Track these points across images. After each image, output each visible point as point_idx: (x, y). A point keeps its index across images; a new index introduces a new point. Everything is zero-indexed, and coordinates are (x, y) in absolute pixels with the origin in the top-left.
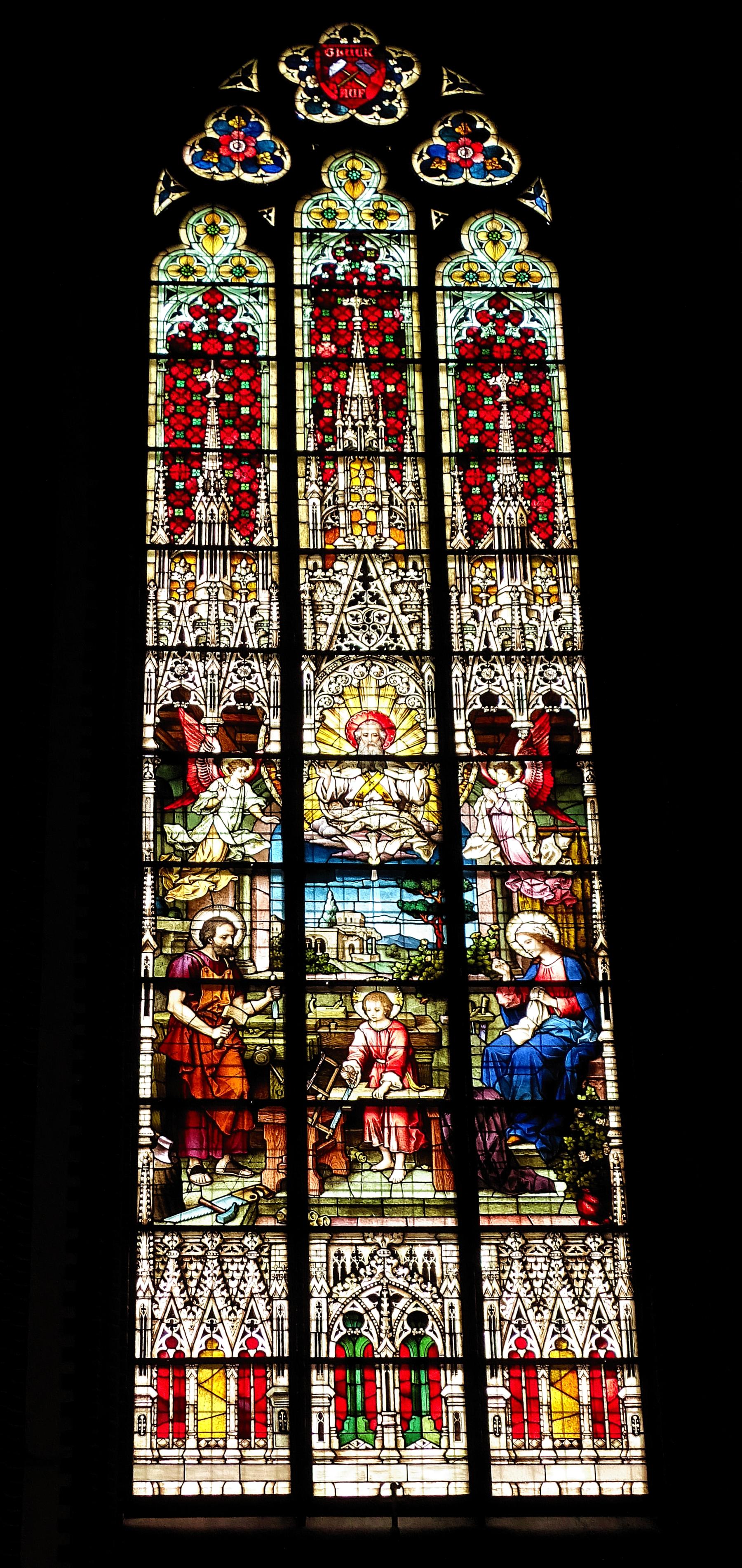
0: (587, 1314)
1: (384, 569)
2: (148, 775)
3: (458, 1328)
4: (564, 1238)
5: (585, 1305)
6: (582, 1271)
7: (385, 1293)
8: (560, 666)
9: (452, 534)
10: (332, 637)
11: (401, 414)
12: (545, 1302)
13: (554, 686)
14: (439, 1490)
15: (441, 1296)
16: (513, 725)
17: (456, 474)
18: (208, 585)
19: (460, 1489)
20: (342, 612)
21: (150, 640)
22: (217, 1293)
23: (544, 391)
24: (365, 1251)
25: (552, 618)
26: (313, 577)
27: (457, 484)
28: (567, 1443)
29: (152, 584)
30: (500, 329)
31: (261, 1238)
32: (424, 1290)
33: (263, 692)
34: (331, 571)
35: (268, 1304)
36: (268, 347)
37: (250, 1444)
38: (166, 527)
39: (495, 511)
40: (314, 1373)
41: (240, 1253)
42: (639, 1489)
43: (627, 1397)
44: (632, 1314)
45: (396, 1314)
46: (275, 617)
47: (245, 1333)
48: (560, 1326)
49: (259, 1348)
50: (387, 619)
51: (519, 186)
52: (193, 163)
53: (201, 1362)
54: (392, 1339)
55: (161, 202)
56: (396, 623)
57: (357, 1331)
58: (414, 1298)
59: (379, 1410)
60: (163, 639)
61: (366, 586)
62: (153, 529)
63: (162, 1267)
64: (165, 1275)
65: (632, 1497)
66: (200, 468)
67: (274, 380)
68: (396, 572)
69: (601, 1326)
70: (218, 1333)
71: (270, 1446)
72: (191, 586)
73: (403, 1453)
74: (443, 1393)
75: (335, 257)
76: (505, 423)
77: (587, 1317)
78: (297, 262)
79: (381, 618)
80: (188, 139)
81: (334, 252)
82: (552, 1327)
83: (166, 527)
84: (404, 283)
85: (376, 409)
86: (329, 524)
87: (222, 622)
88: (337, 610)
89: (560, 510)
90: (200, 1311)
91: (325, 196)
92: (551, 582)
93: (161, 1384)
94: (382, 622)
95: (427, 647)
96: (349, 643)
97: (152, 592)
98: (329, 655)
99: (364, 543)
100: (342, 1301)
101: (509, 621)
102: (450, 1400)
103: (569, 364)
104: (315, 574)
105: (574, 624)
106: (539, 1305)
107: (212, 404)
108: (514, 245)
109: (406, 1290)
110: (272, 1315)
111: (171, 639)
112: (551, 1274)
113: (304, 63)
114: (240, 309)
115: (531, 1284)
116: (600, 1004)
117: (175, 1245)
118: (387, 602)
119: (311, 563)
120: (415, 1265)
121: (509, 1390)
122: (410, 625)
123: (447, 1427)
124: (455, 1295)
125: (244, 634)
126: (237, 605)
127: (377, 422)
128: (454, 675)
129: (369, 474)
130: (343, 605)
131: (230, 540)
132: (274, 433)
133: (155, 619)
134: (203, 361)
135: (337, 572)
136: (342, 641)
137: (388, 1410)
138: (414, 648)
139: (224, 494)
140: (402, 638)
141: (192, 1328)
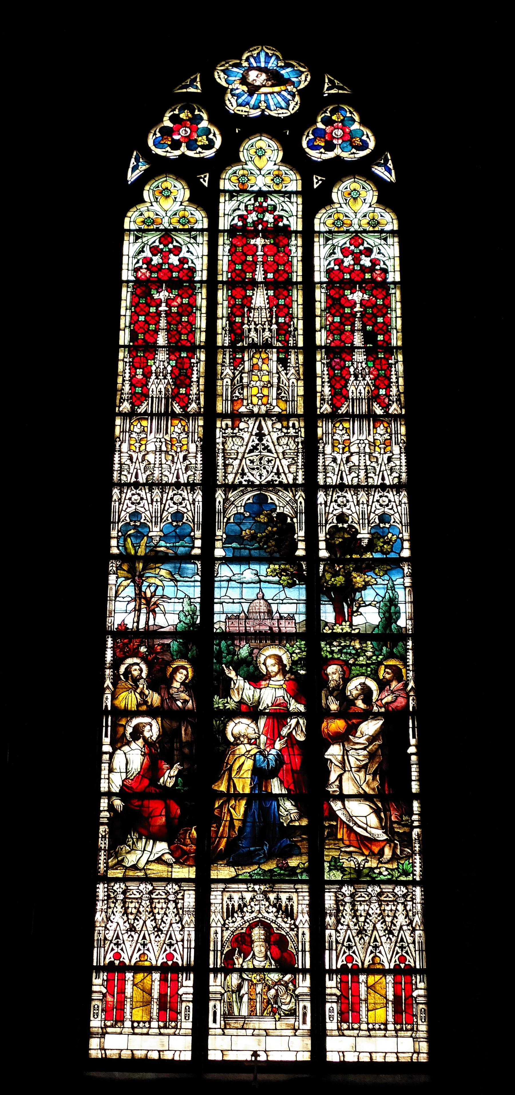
0: (394, 939)
1: (273, 428)
5: (162, 931)
8: (185, 494)
9: (121, 402)
10: (236, 474)
12: (366, 932)
14: (290, 1057)
15: (297, 927)
16: (359, 536)
23: (191, 303)
26: (225, 433)
30: (357, 260)
32: (286, 923)
33: (397, 515)
34: (237, 429)
37: (177, 1025)
39: (351, 388)
42: (423, 1058)
44: (423, 939)
46: (404, 464)
47: (165, 950)
50: (273, 462)
55: (133, 172)
56: (279, 465)
61: (260, 440)
62: (321, 404)
63: (112, 905)
64: (344, 914)
65: (419, 1063)
66: (351, 360)
67: (204, 296)
68: (280, 430)
69: (170, 945)
70: (148, 950)
71: (179, 1027)
75: (246, 210)
79: (269, 461)
80: (151, 128)
81: (246, 207)
82: (139, 945)
84: (293, 228)
85: (271, 316)
86: (236, 396)
87: (368, 467)
88: (240, 457)
90: (137, 935)
91: (241, 167)
93: (109, 983)
94: (270, 464)
96: (247, 479)
97: (321, 447)
100: (232, 929)
101: (357, 464)
102: (184, 996)
104: (227, 431)
105: (401, 466)
108: (369, 200)
114: (375, 249)
115: (357, 919)
117: (121, 890)
118: (274, 451)
119: (224, 423)
120: (280, 905)
121: (340, 991)
122: (289, 467)
124: (192, 925)
127: (271, 326)
130: (244, 453)
133: (324, 465)
135: (241, 430)
136: (242, 478)
138: (291, 482)
140: (283, 475)
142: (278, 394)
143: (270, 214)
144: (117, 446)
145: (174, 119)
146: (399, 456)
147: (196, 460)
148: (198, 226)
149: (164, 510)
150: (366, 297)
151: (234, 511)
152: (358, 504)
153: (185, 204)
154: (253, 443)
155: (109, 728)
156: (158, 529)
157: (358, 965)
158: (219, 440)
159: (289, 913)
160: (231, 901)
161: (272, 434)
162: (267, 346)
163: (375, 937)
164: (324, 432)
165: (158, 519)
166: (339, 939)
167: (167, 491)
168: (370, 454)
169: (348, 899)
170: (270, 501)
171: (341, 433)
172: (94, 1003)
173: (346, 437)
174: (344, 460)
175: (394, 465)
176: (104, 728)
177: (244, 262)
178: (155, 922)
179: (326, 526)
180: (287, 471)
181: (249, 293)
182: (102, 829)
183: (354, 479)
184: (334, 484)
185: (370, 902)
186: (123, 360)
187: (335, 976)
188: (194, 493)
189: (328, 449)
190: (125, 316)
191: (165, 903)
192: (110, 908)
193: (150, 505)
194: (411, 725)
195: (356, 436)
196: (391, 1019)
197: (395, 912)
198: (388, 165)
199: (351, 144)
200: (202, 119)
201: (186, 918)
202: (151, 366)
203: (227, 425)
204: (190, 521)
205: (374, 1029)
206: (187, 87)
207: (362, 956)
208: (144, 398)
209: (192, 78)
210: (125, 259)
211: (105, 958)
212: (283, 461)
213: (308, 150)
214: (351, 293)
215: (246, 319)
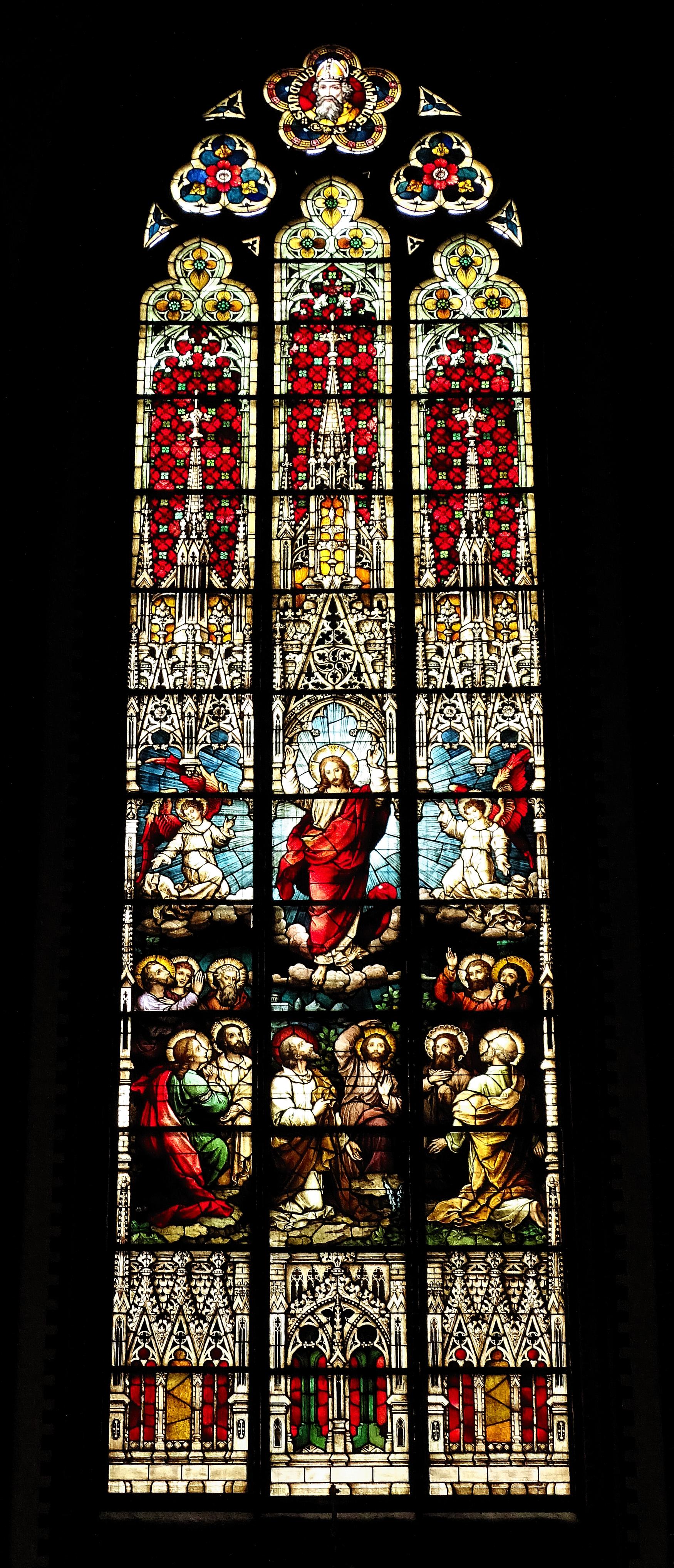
0: (522, 1327)
6: (518, 1288)
11: (511, 448)
12: (484, 1317)
18: (472, 625)
19: (401, 1489)
21: (132, 683)
27: (427, 523)
28: (499, 1447)
29: (420, 626)
32: (374, 1306)
35: (230, 1318)
36: (249, 385)
38: (433, 570)
45: (347, 1327)
47: (527, 1345)
48: (180, 1337)
49: (467, 1359)
52: (398, 193)
57: (312, 1345)
58: (364, 1313)
59: (331, 1417)
61: (333, 626)
63: (136, 1284)
64: (140, 1292)
68: (361, 611)
69: (533, 1339)
72: (170, 629)
73: (294, 1457)
74: (389, 1402)
76: (472, 458)
78: (277, 297)
79: (346, 656)
82: (489, 1339)
83: (150, 570)
84: (380, 317)
87: (199, 664)
89: (522, 544)
90: (170, 1324)
91: (303, 224)
92: (512, 617)
98: (299, 694)
101: (471, 657)
102: (395, 1408)
104: (286, 613)
107: (472, 443)
109: (357, 1306)
110: (234, 1329)
115: (157, 1299)
116: (543, 1033)
117: (220, 1263)
118: (352, 642)
120: (366, 1283)
121: (129, 1397)
122: (373, 663)
124: (402, 1310)
126: (213, 647)
128: (418, 712)
131: (494, 581)
132: (253, 472)
133: (138, 661)
134: (459, 399)
136: (309, 680)
138: (377, 686)
141: (163, 1339)
142: (358, 560)
143: (346, 296)
144: (134, 635)
145: (425, 156)
147: (244, 657)
148: (513, 313)
149: (142, 729)
150: (482, 417)
154: (323, 631)
155: (129, 1036)
156: (193, 755)
159: (379, 1294)
160: (297, 1277)
162: (342, 490)
163: (496, 1323)
164: (425, 613)
167: (493, 701)
168: (489, 643)
171: (505, 613)
173: (454, 618)
174: (510, 651)
175: (523, 658)
177: (309, 367)
178: (195, 1307)
179: (137, 748)
180: (370, 670)
183: (236, 681)
184: (207, 687)
186: (140, 512)
187: (283, 1381)
188: (242, 703)
190: (418, 446)
192: (133, 1287)
193: (529, 720)
194: (545, 1030)
195: (183, 618)
196: (517, 1437)
197: (524, 1290)
198: (513, 220)
200: (244, 157)
202: (460, 519)
203: (286, 604)
204: (178, 744)
205: (174, 1449)
206: (224, 109)
209: (231, 97)
210: (412, 363)
213: (397, 199)
214: (187, 412)
215: (312, 450)
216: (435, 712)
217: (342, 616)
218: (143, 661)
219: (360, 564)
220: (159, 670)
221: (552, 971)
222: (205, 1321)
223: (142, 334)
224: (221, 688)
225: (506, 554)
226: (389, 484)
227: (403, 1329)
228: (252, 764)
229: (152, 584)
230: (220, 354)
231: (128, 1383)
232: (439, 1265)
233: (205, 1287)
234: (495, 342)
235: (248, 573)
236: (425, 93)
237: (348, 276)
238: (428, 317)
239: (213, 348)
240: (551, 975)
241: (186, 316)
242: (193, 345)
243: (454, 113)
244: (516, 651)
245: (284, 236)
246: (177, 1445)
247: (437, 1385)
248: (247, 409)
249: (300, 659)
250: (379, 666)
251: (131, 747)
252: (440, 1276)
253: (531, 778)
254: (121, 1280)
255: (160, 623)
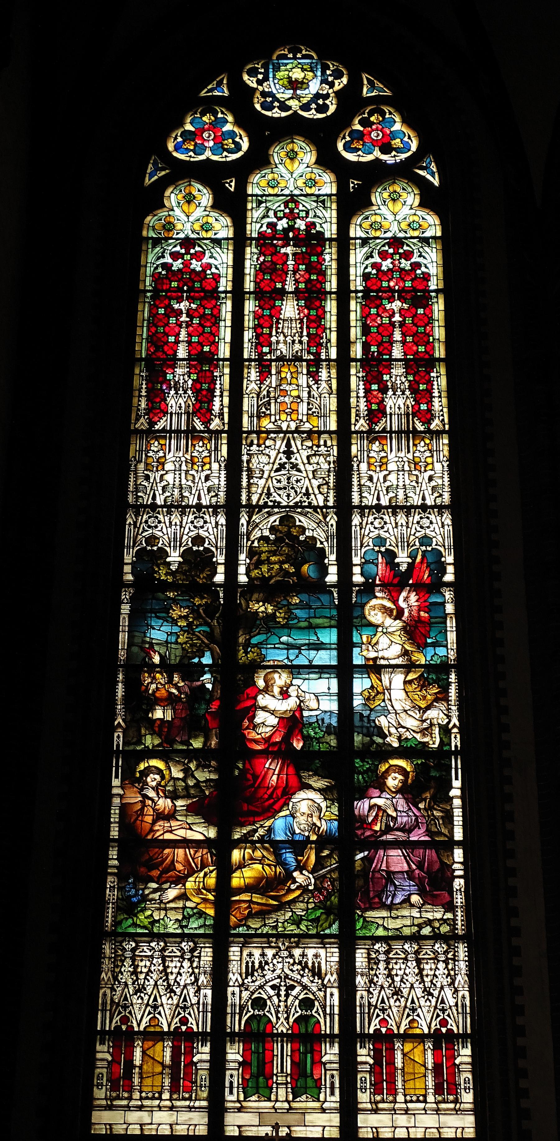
0: (434, 1001)
1: (302, 445)
2: (125, 601)
3: (336, 1010)
4: (135, 942)
5: (432, 995)
6: (431, 969)
7: (283, 984)
9: (357, 420)
10: (261, 495)
13: (428, 531)
16: (168, 559)
17: (360, 375)
19: (202, 1131)
20: (269, 476)
21: (131, 499)
22: (160, 982)
23: (215, 313)
24: (270, 953)
25: (203, 481)
26: (250, 450)
27: (361, 383)
31: (447, 945)
36: (225, 284)
37: (191, 1096)
40: (228, 1045)
41: (432, 956)
43: (461, 1063)
45: (291, 998)
46: (447, 483)
47: (179, 1014)
49: (449, 1027)
50: (302, 482)
51: (415, 160)
53: (406, 1037)
54: (287, 1019)
58: (305, 987)
60: (186, 500)
61: (289, 458)
63: (120, 964)
64: (122, 970)
69: (185, 1008)
72: (385, 460)
73: (245, 1104)
74: (323, 1060)
75: (276, 216)
77: (433, 1004)
79: (298, 481)
81: (275, 213)
84: (327, 235)
85: (301, 328)
88: (266, 475)
89: (436, 400)
90: (147, 997)
92: (428, 454)
94: (299, 484)
95: (331, 503)
97: (355, 465)
99: (288, 426)
102: (328, 1066)
103: (445, 291)
106: (397, 994)
110: (199, 1001)
111: (370, 500)
112: (407, 972)
113: (261, 73)
116: (451, 768)
117: (384, 950)
120: (306, 963)
121: (111, 1055)
122: (319, 487)
123: (325, 1085)
125: (199, 495)
129: (294, 375)
130: (271, 471)
131: (414, 427)
135: (268, 447)
136: (268, 498)
137: (282, 1072)
138: (321, 504)
139: (190, 392)
140: (312, 496)
141: (428, 1012)
146: (217, 475)
149: (138, 534)
150: (406, 306)
151: (259, 535)
152: (443, 526)
153: (208, 209)
157: (192, 1029)
158: (245, 458)
161: (300, 451)
165: (176, 542)
166: (371, 1000)
169: (128, 954)
170: (298, 523)
171: (422, 450)
172: (98, 1071)
173: (161, 454)
176: (114, 769)
181: (278, 303)
182: (110, 879)
185: (408, 961)
189: (364, 467)
191: (434, 963)
192: (117, 966)
199: (222, 147)
201: (202, 979)
207: (397, 1019)
208: (380, 415)
211: (111, 1022)
212: (313, 481)
215: (274, 329)
216: (367, 524)
217: (295, 451)
218: (140, 484)
219: (310, 412)
220: (377, 492)
221: (459, 720)
222: (175, 994)
223: (144, 248)
224: (156, 504)
225: (424, 407)
226: (333, 355)
227: (336, 1002)
228: (223, 561)
229: (368, 428)
230: (413, 260)
231: (371, 1047)
232: (366, 951)
233: (431, 969)
234: (416, 255)
235: (223, 419)
236: (367, 78)
237: (304, 206)
238: (363, 235)
239: (199, 256)
240: (458, 724)
241: (177, 234)
242: (392, 254)
243: (388, 93)
244: (207, 478)
245: (255, 178)
246: (150, 1095)
247: (365, 1047)
248: (224, 301)
249: (262, 482)
250: (324, 489)
251: (129, 547)
252: (366, 960)
253: (444, 572)
254: (107, 960)
255: (376, 456)
